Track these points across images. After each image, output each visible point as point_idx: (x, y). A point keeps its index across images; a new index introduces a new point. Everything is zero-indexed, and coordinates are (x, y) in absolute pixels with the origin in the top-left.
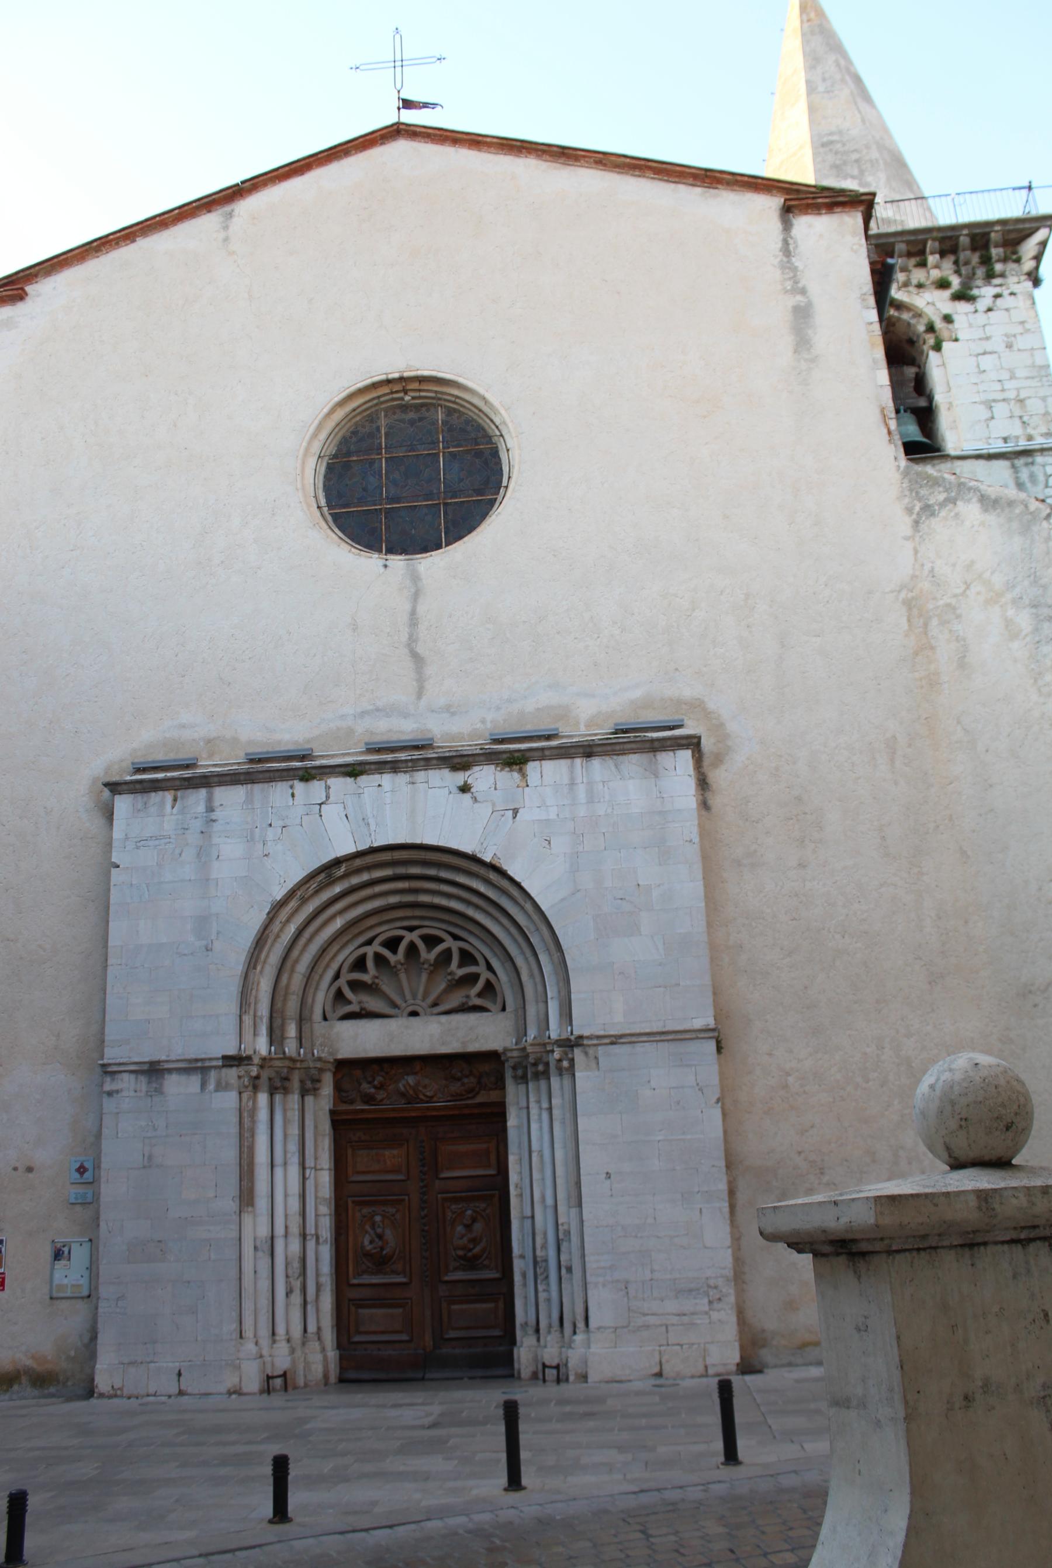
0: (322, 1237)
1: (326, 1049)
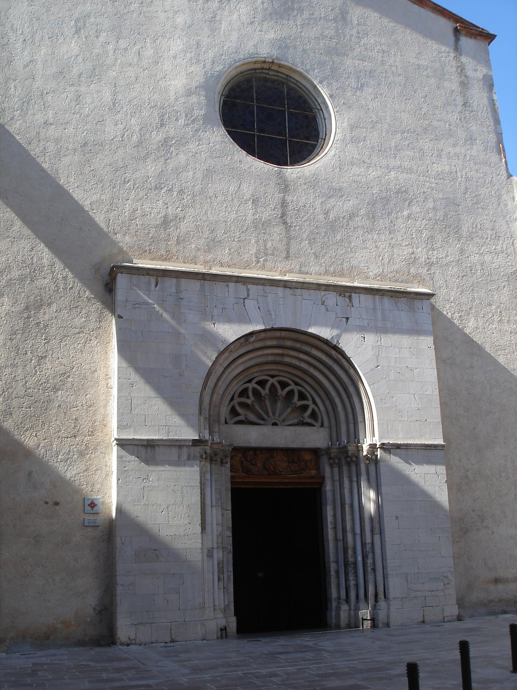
1: (228, 440)
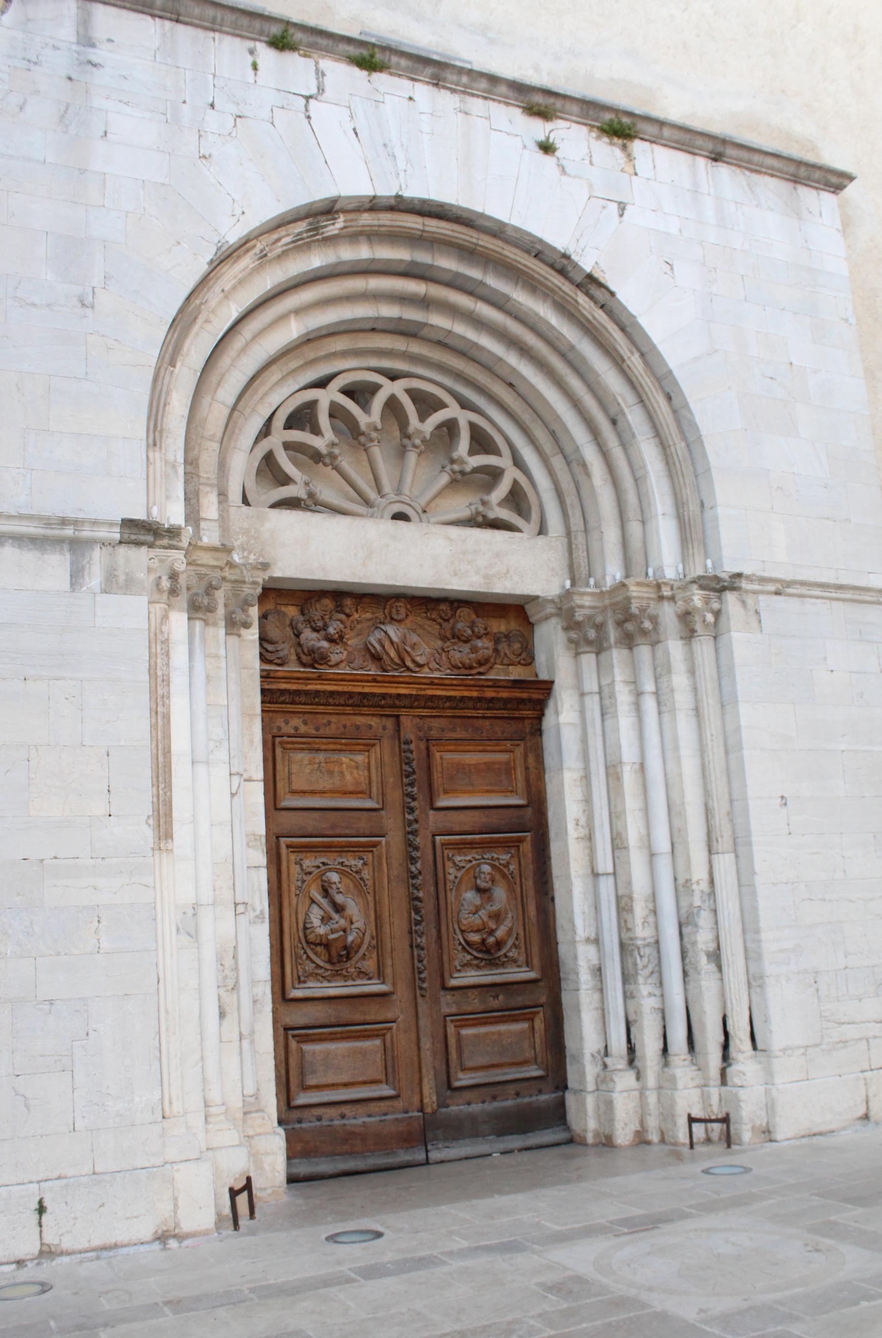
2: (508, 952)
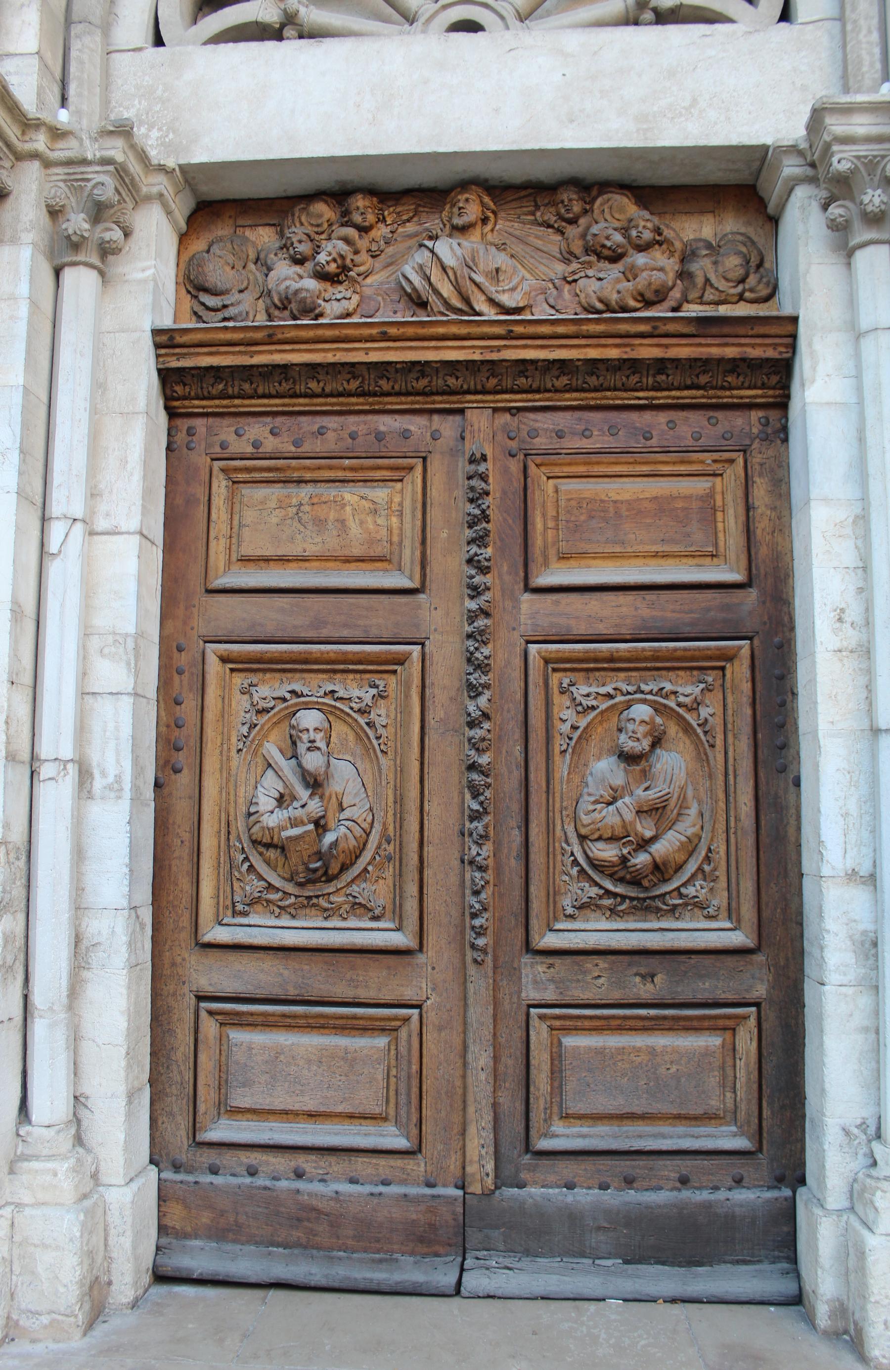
0: (104, 774)
2: (684, 885)
